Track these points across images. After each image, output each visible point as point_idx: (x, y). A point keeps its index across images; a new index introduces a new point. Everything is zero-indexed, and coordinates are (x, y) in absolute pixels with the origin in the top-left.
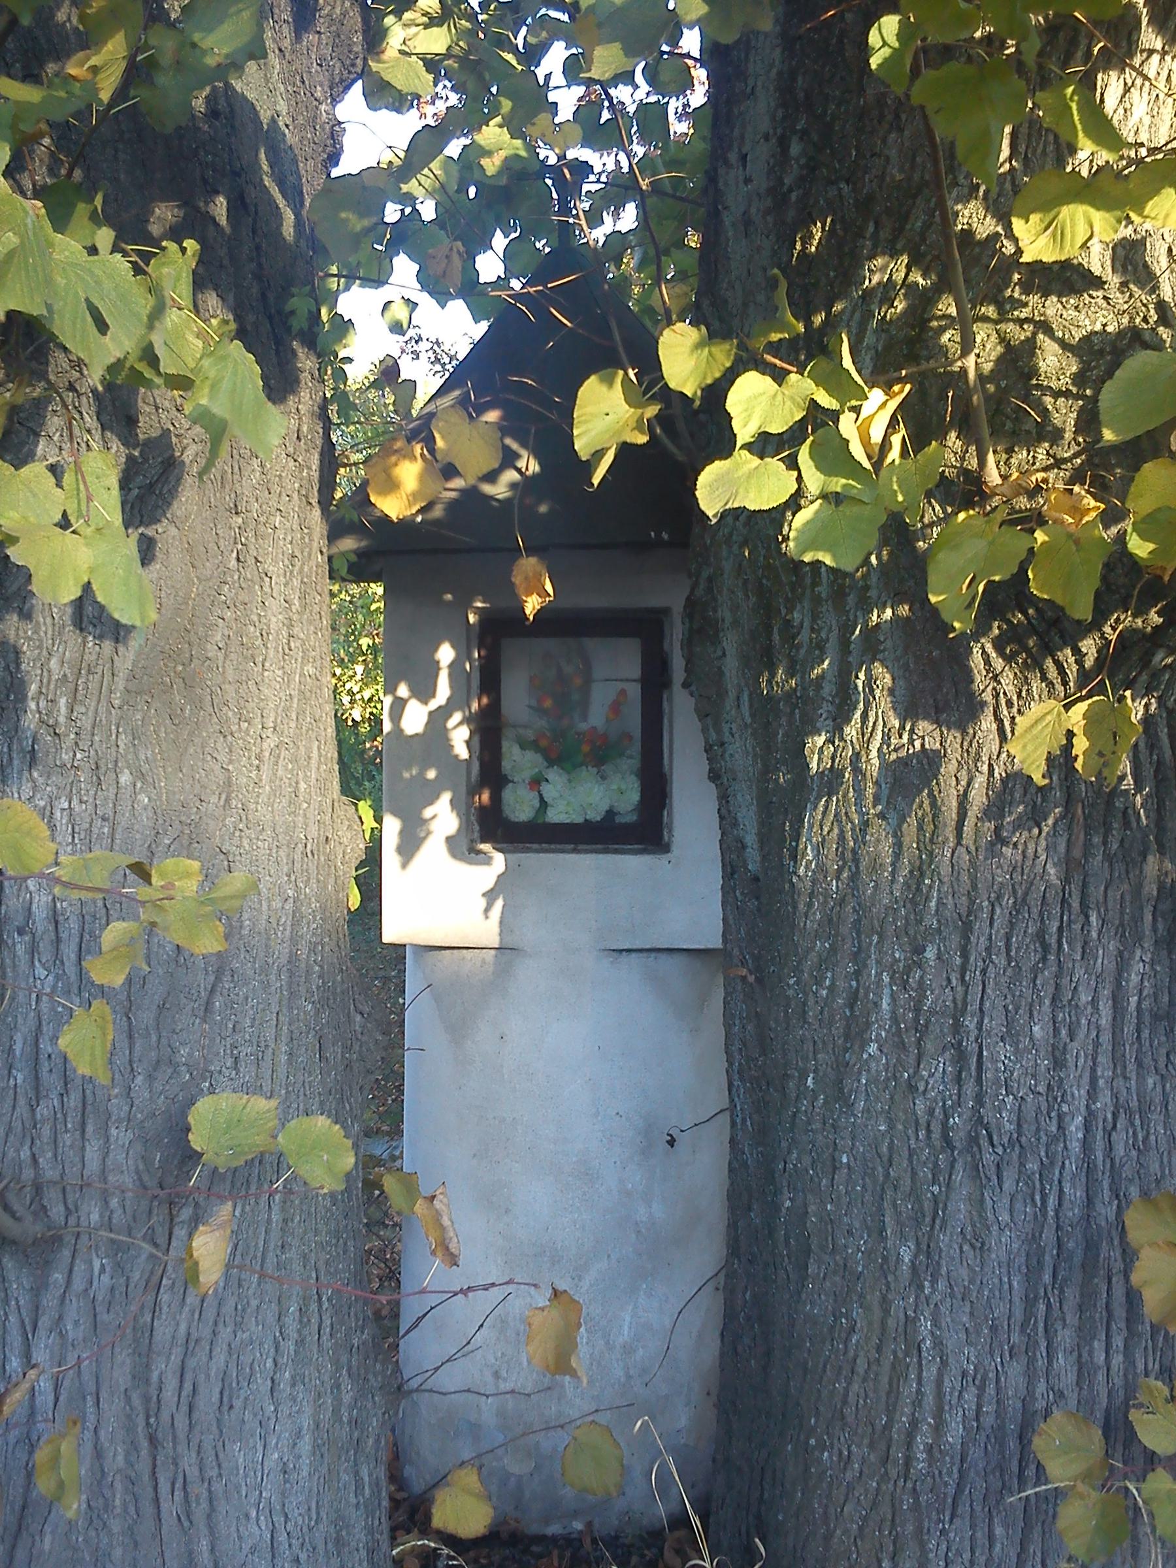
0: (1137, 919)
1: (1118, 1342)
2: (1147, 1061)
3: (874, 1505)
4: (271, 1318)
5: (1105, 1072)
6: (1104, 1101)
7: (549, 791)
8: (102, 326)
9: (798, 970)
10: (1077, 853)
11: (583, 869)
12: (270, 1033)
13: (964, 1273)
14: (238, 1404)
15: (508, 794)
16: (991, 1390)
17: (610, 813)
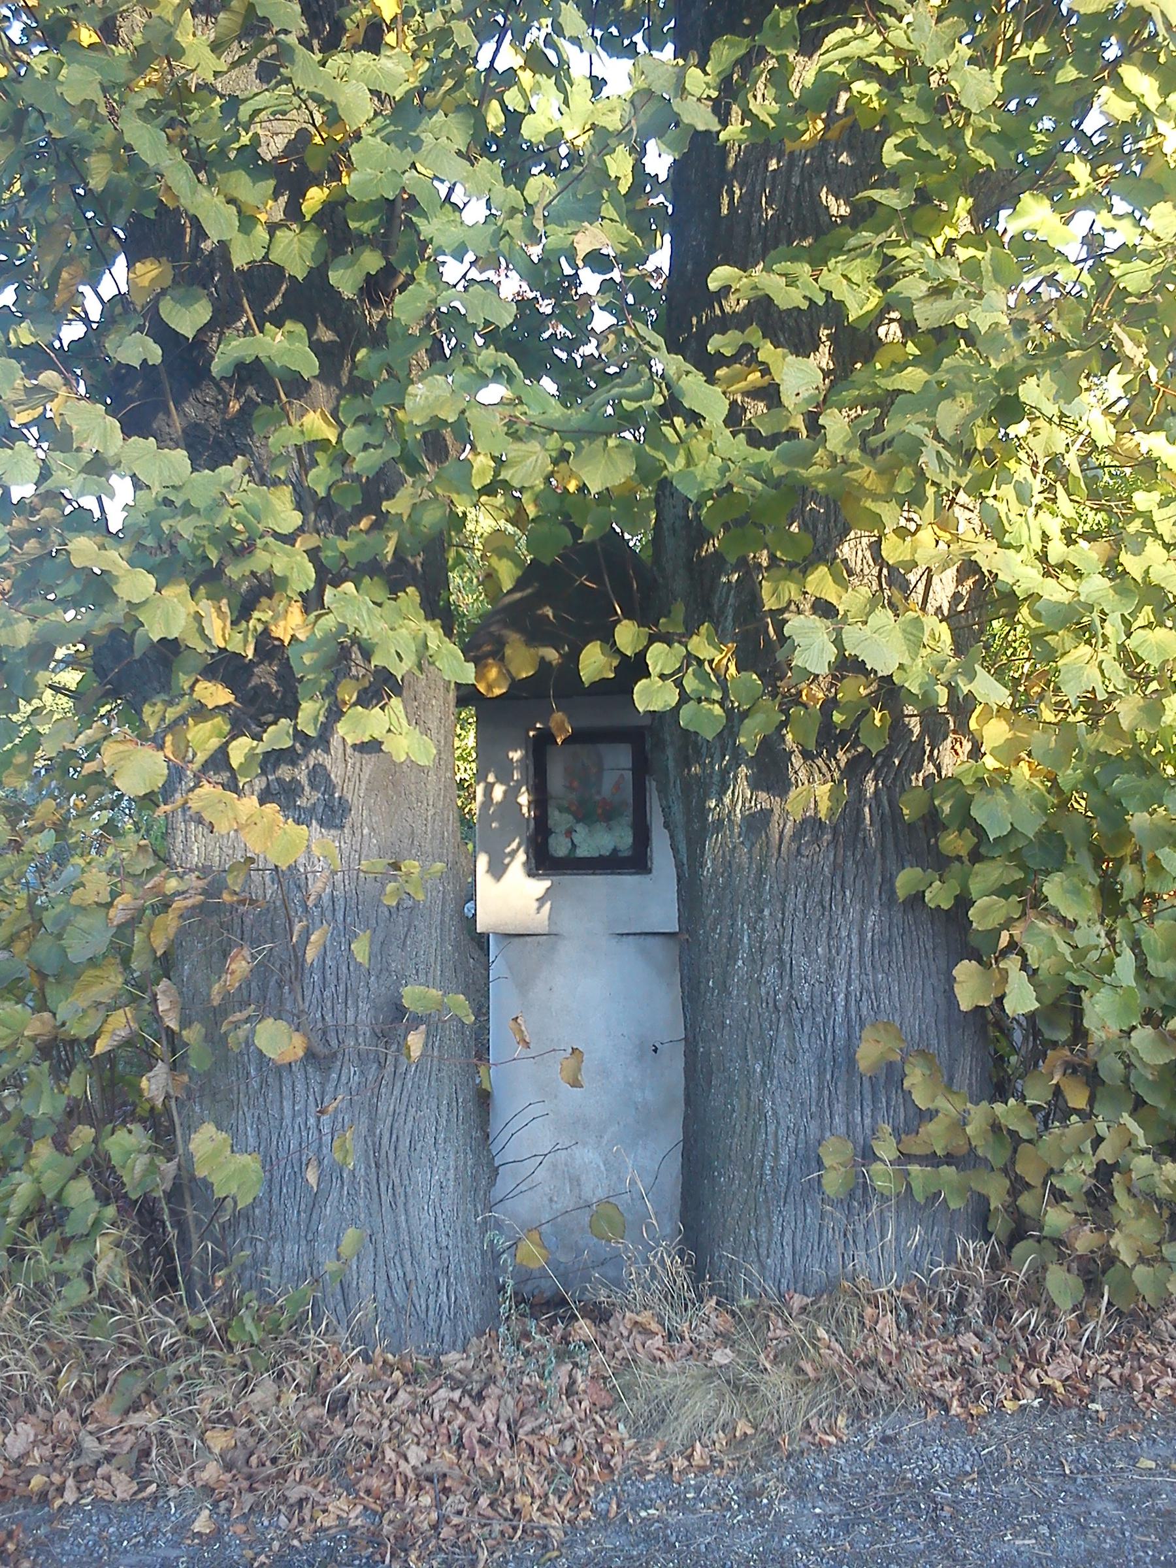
0: (871, 893)
1: (868, 1111)
2: (878, 965)
3: (746, 1202)
4: (434, 1107)
5: (855, 971)
6: (856, 985)
7: (577, 838)
8: (401, 659)
9: (704, 926)
10: (839, 861)
11: (597, 884)
12: (432, 960)
13: (787, 1076)
14: (419, 1147)
15: (552, 841)
16: (802, 1135)
17: (615, 850)
